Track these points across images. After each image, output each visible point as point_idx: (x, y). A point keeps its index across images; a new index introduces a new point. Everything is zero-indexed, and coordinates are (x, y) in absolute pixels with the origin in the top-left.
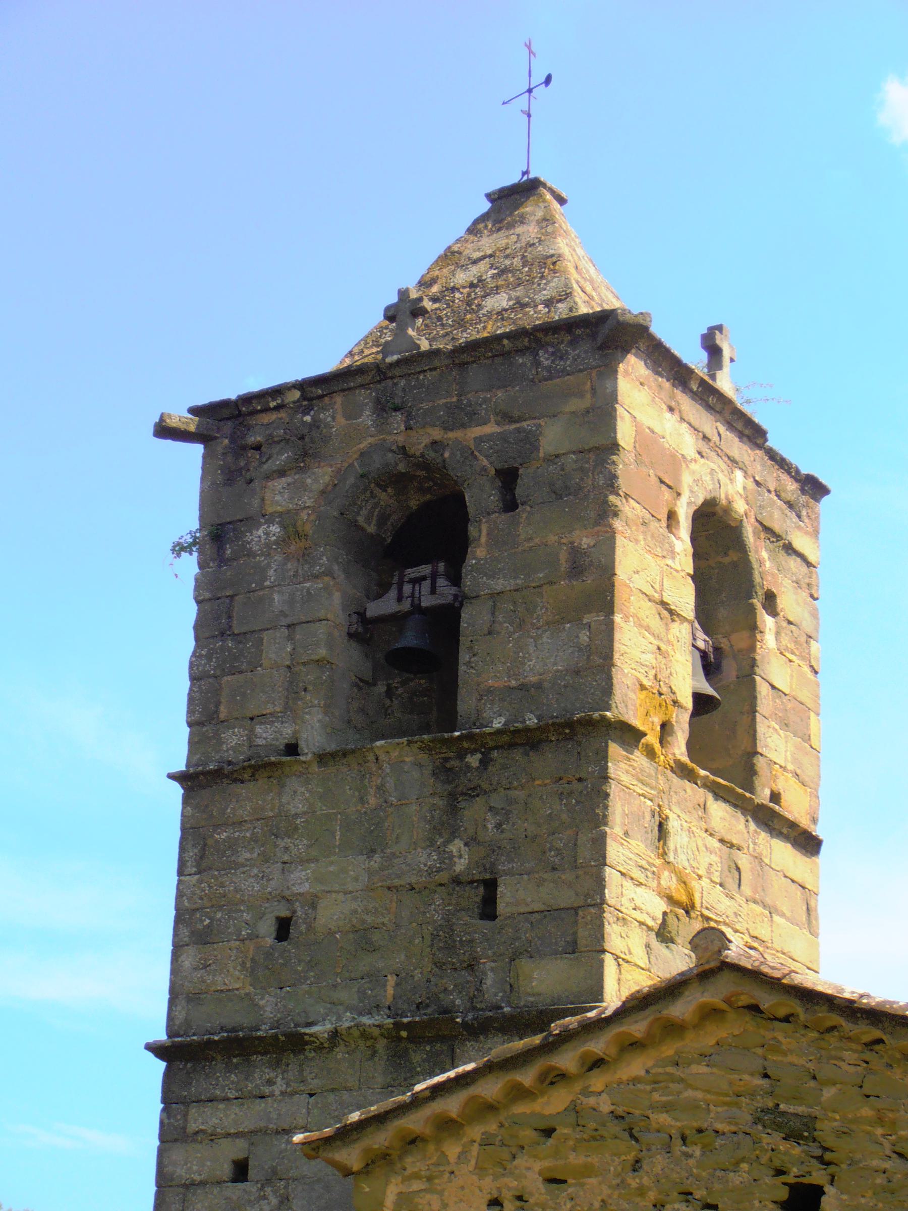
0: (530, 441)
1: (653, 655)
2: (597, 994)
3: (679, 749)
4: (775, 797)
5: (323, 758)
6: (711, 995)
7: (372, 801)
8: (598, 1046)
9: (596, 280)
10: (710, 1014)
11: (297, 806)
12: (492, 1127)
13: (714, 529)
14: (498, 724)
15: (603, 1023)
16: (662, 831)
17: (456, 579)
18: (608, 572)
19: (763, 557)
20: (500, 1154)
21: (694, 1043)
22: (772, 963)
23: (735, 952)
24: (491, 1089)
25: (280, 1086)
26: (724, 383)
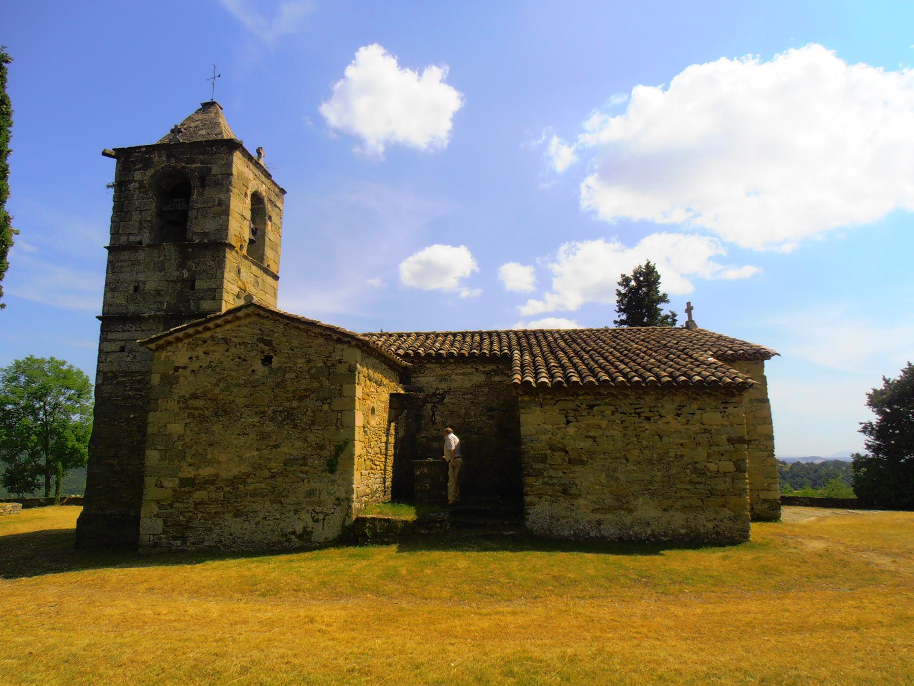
0: (210, 169)
1: (239, 227)
2: (220, 310)
3: (245, 252)
4: (268, 266)
5: (149, 246)
6: (250, 310)
7: (162, 258)
8: (219, 322)
9: (229, 131)
10: (248, 315)
11: (141, 258)
12: (191, 340)
13: (257, 199)
14: (197, 241)
15: (220, 316)
16: (239, 272)
17: (188, 203)
18: (228, 206)
19: (269, 207)
20: (192, 346)
21: (243, 322)
22: (264, 304)
23: (255, 300)
24: (191, 331)
25: (134, 328)
26: (262, 162)
